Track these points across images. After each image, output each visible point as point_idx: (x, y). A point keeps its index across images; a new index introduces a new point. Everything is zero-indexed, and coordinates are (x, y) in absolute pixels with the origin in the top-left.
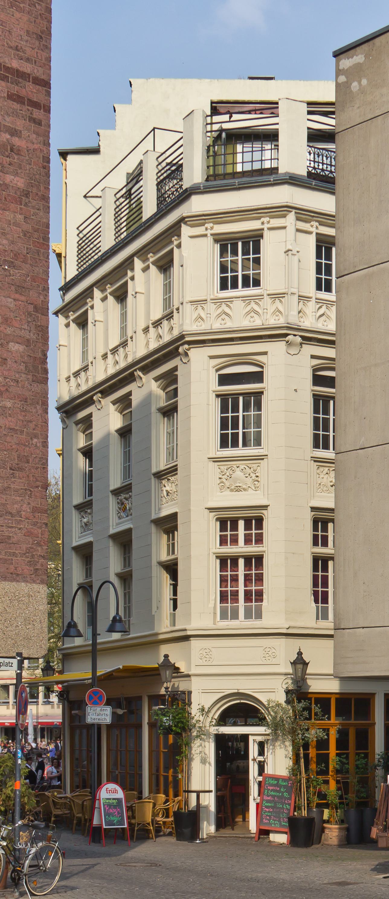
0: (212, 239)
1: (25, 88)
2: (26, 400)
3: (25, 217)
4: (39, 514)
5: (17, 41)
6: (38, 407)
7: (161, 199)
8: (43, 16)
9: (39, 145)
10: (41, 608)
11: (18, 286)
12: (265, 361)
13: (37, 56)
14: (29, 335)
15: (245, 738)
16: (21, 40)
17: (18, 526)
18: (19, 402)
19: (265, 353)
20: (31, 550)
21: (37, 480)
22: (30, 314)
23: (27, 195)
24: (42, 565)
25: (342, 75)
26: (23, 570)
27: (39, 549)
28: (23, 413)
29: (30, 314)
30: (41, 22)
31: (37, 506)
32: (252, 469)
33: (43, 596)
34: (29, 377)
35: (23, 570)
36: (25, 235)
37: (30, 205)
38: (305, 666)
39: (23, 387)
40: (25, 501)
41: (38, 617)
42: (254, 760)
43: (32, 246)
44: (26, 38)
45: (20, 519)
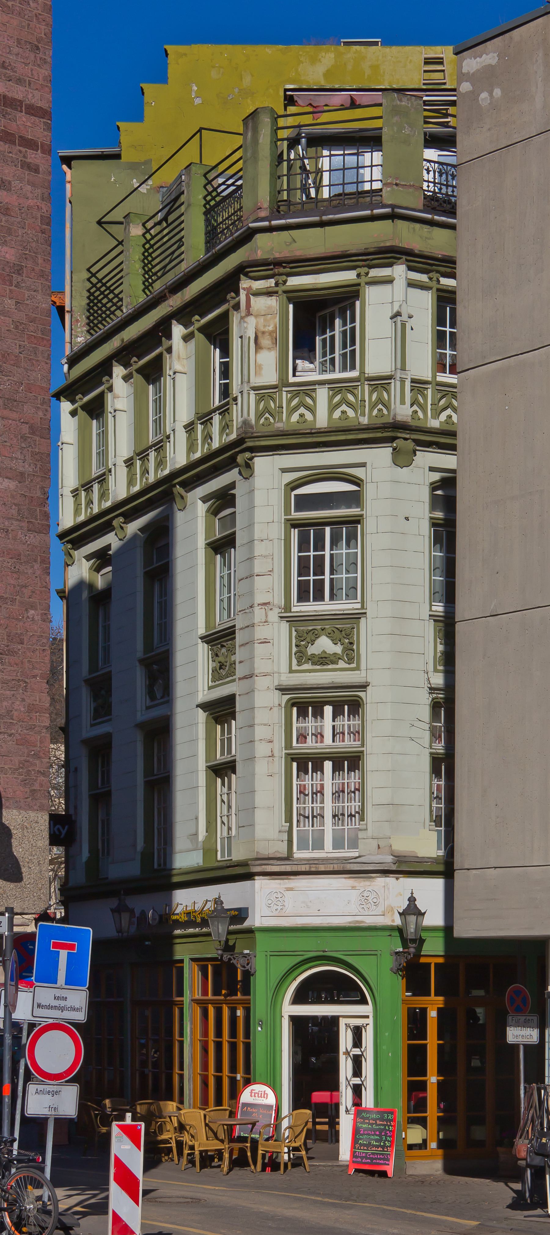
0: (285, 298)
1: (15, 121)
2: (18, 556)
3: (17, 303)
4: (38, 714)
5: (4, 54)
6: (37, 566)
7: (212, 235)
8: (40, 17)
9: (36, 201)
10: (40, 844)
11: (8, 399)
12: (363, 477)
13: (32, 75)
14: (24, 467)
15: (334, 1021)
16: (10, 53)
17: (9, 731)
18: (9, 560)
19: (363, 465)
20: (26, 764)
21: (34, 668)
22: (24, 438)
23: (19, 272)
24: (41, 785)
25: (467, 81)
26: (14, 792)
27: (37, 762)
28: (15, 576)
29: (24, 438)
30: (38, 25)
31: (34, 703)
32: (343, 632)
33: (43, 827)
34: (23, 524)
35: (14, 792)
36: (16, 327)
37: (23, 285)
38: (420, 918)
39: (15, 539)
40: (18, 696)
41: (36, 857)
42: (347, 1053)
43: (26, 343)
44: (16, 50)
45: (11, 721)
